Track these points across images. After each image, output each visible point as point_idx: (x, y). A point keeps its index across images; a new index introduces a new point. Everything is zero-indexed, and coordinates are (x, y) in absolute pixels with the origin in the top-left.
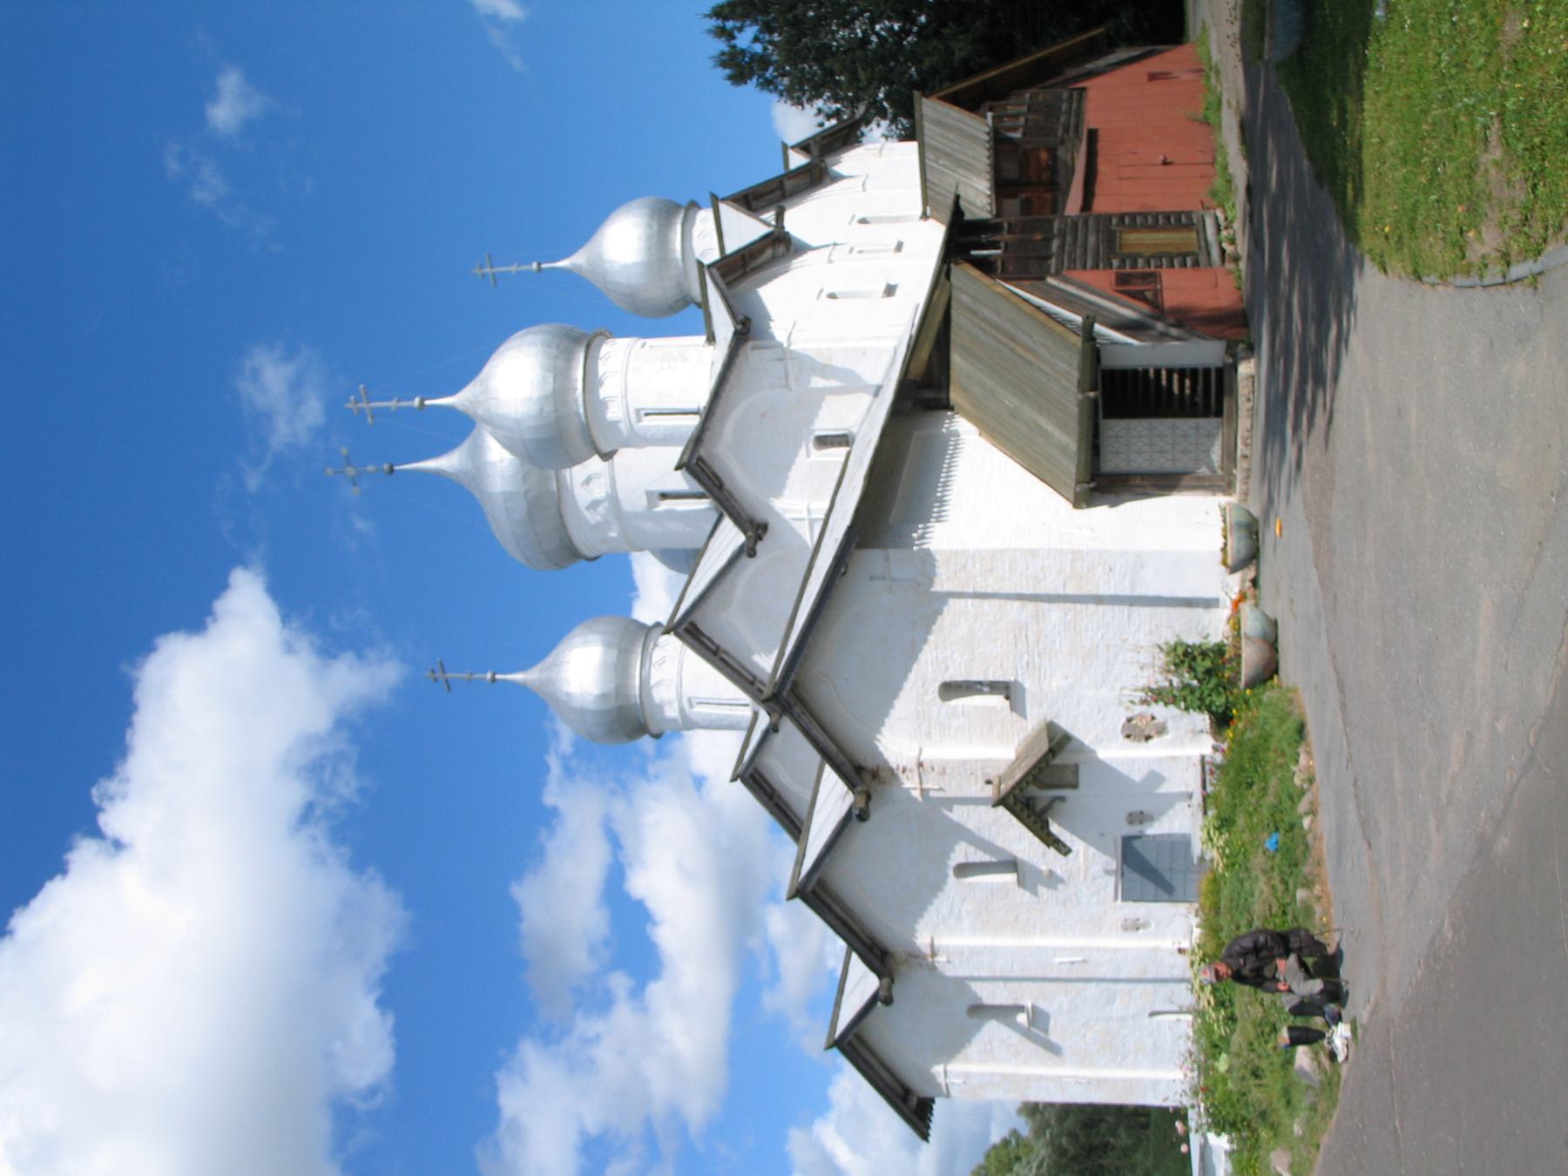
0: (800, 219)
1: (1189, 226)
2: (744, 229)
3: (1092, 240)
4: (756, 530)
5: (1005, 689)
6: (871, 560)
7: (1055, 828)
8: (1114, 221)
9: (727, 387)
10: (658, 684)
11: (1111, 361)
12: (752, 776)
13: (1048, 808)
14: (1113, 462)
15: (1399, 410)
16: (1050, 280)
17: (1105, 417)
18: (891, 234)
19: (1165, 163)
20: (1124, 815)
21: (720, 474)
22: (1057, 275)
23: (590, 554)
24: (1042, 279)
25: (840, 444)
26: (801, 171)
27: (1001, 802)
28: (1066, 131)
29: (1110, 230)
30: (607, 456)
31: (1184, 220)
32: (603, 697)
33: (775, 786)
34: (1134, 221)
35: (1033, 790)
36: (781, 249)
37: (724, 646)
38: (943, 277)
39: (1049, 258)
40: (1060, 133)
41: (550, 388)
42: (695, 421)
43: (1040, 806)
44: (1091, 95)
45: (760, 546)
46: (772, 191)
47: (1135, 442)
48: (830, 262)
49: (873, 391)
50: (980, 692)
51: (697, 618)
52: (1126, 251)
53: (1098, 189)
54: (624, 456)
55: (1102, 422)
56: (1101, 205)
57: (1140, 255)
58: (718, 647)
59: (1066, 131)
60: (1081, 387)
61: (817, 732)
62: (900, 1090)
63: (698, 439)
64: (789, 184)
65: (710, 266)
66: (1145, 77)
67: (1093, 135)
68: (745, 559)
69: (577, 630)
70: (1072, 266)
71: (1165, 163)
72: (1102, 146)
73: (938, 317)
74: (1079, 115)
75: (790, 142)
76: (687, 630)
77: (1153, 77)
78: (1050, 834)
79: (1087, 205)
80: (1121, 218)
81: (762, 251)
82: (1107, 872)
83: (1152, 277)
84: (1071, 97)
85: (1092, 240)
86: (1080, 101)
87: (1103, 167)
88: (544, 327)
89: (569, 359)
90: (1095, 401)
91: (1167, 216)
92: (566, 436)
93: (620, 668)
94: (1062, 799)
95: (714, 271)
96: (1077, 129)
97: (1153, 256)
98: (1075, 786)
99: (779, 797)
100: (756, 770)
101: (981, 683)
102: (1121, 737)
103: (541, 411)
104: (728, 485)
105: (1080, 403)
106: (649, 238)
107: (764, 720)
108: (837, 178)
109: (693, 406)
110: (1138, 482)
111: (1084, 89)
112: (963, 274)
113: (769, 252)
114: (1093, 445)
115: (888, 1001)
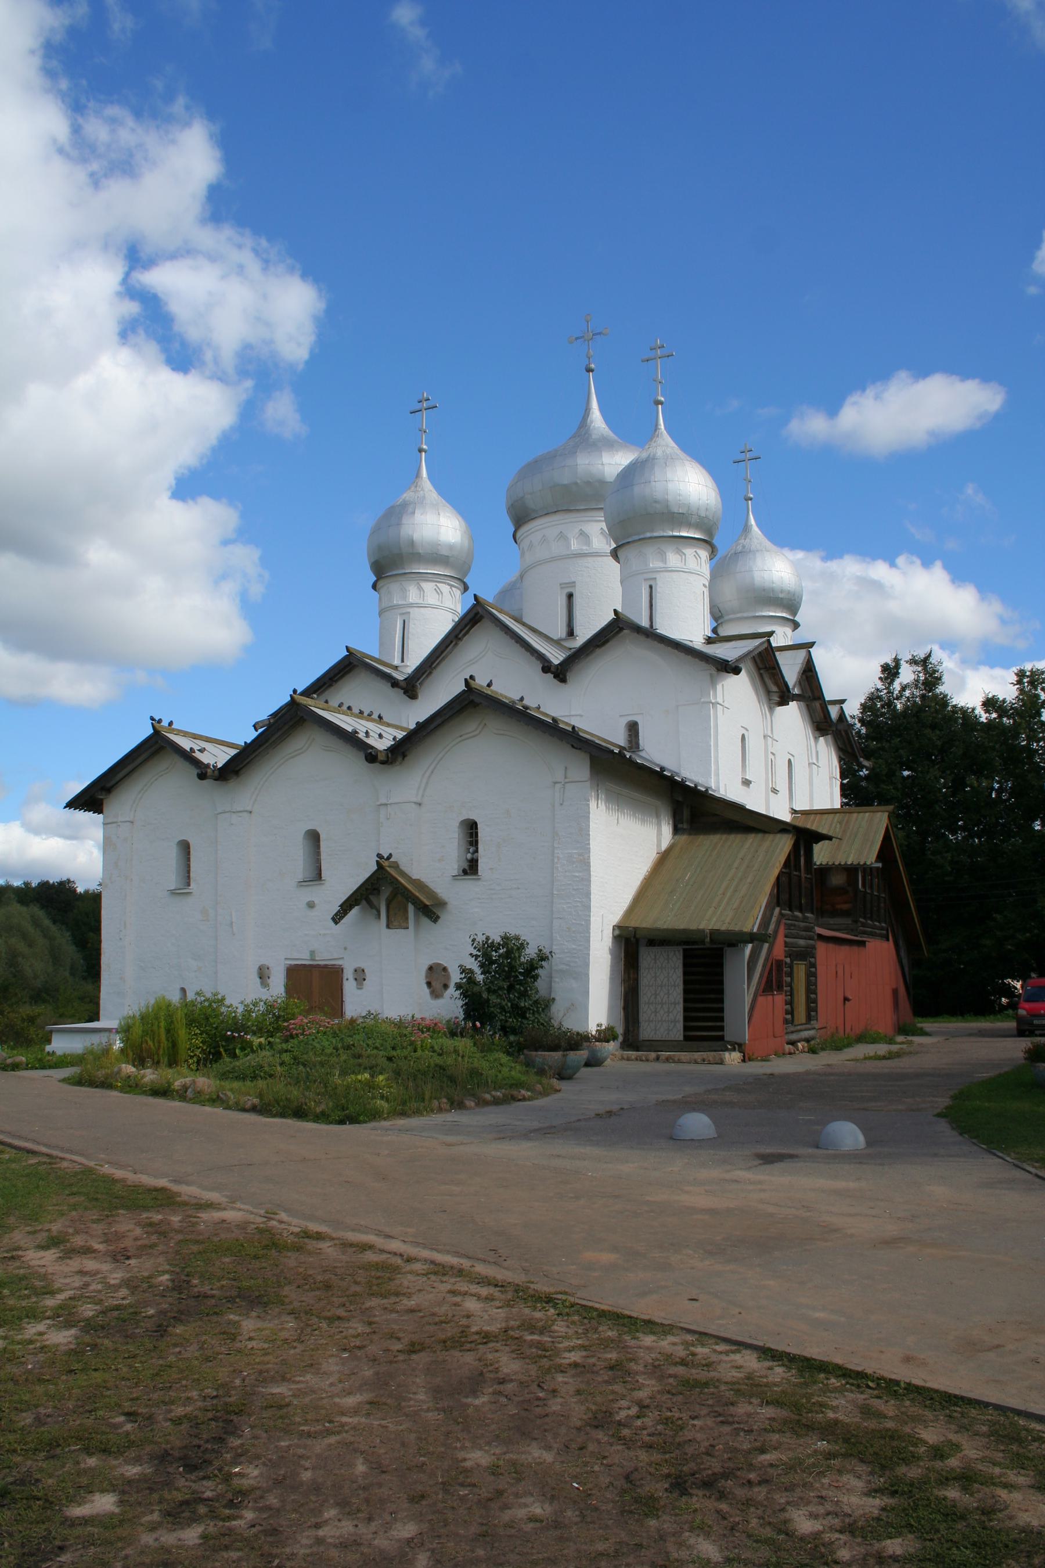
0: (792, 714)
1: (809, 1018)
3: (802, 942)
5: (471, 868)
6: (580, 768)
7: (355, 911)
8: (812, 960)
9: (682, 655)
10: (420, 589)
11: (728, 952)
12: (350, 663)
13: (371, 905)
14: (647, 957)
16: (777, 910)
17: (684, 950)
18: (782, 785)
19: (846, 999)
20: (362, 965)
21: (608, 645)
22: (781, 914)
23: (518, 535)
24: (778, 904)
25: (630, 742)
26: (826, 714)
29: (805, 955)
30: (615, 554)
31: (813, 1014)
32: (412, 543)
33: (340, 683)
34: (811, 976)
35: (386, 892)
36: (776, 698)
37: (461, 643)
38: (782, 827)
39: (790, 910)
42: (644, 623)
43: (372, 898)
45: (550, 676)
46: (812, 691)
47: (665, 981)
48: (765, 737)
51: (486, 623)
52: (795, 967)
53: (831, 946)
54: (613, 567)
55: (681, 948)
56: (821, 948)
57: (792, 979)
58: (460, 639)
60: (713, 932)
61: (439, 721)
62: (109, 785)
63: (650, 635)
64: (817, 704)
65: (769, 641)
67: (862, 944)
68: (539, 666)
69: (463, 524)
70: (788, 927)
71: (846, 999)
72: (855, 948)
73: (751, 824)
74: (873, 935)
76: (477, 614)
78: (351, 908)
79: (821, 937)
80: (814, 965)
81: (776, 684)
82: (312, 953)
83: (780, 988)
84: (882, 929)
85: (802, 942)
86: (881, 936)
87: (845, 949)
88: (720, 506)
90: (703, 942)
91: (815, 1001)
92: (641, 525)
93: (437, 557)
95: (766, 645)
96: (864, 933)
97: (792, 988)
98: (388, 927)
99: (331, 686)
100: (355, 666)
101: (476, 851)
102: (431, 963)
103: (656, 502)
104: (598, 651)
105: (703, 931)
106: (773, 590)
107: (400, 677)
108: (816, 739)
111: (888, 940)
112: (784, 844)
113: (774, 688)
114: (660, 940)
115: (202, 776)
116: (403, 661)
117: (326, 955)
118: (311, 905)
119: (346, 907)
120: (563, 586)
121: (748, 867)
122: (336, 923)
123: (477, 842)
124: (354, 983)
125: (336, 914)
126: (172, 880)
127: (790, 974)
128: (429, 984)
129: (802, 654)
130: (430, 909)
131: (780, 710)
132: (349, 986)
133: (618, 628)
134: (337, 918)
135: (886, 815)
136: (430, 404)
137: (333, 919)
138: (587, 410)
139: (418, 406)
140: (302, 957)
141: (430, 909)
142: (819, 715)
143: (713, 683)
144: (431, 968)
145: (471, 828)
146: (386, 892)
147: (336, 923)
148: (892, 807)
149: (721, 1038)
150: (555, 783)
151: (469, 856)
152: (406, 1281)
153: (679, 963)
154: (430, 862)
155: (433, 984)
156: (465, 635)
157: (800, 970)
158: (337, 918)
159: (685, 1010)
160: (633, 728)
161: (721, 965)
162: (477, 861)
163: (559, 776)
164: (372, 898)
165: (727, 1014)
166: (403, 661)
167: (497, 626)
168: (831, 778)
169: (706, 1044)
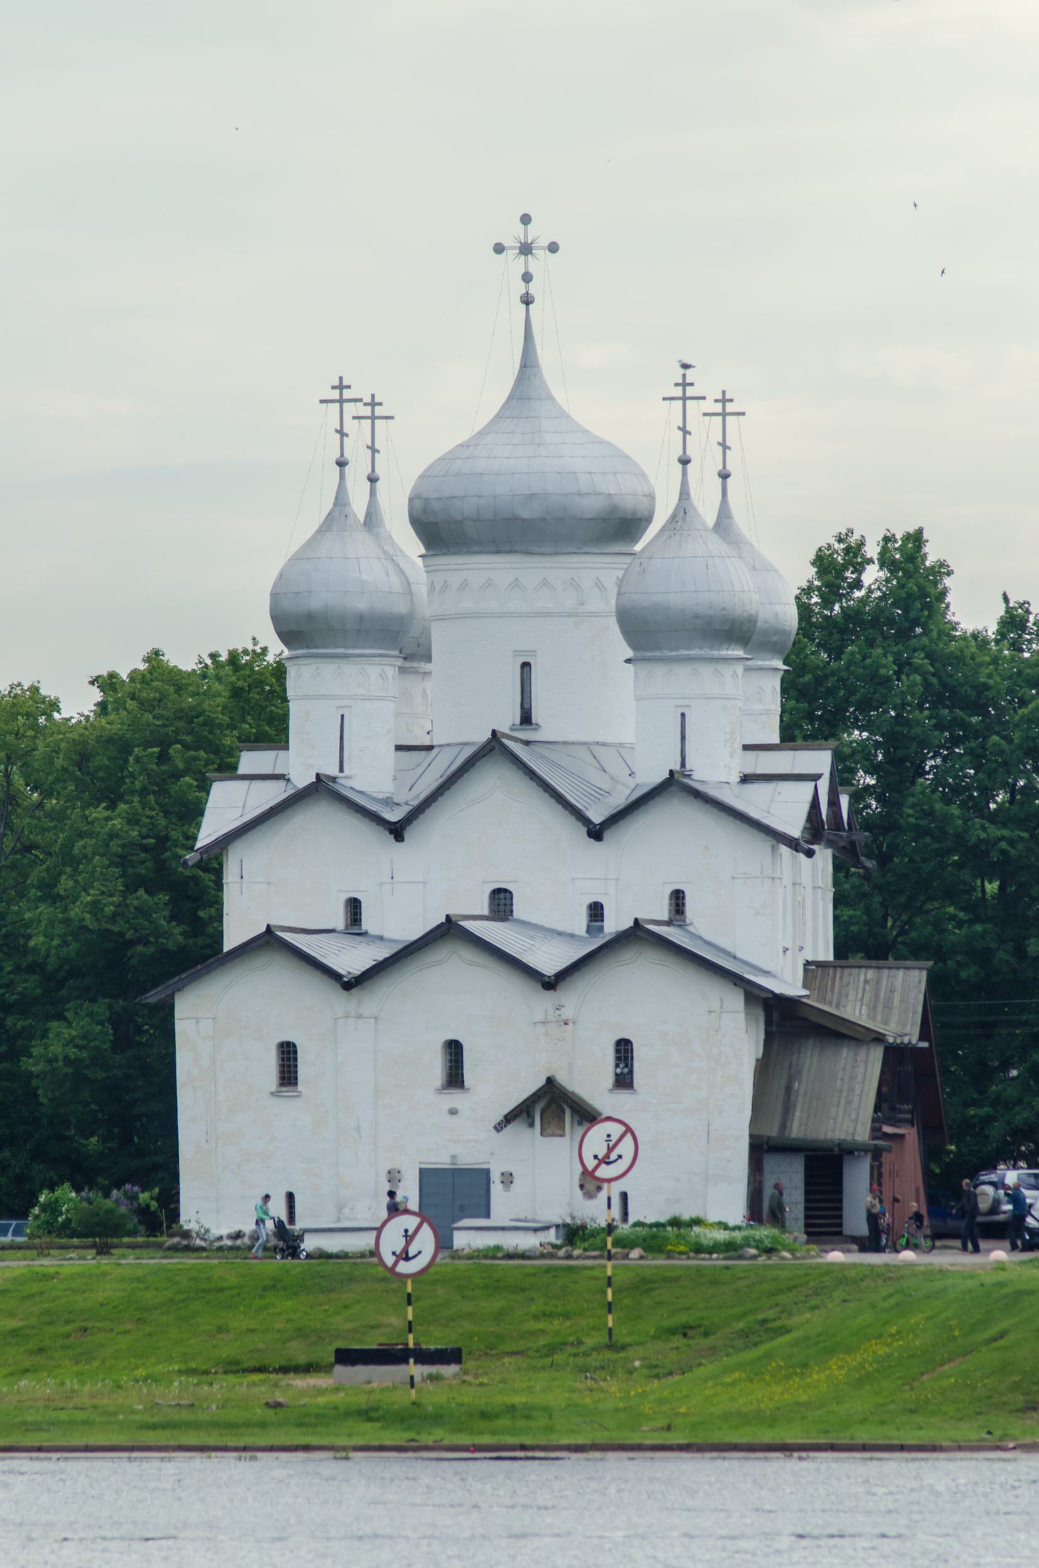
4: (596, 833)
19: (896, 1200)
38: (875, 1035)
47: (790, 1179)
55: (803, 1155)
73: (844, 1031)
82: (454, 1157)
90: (832, 1150)
116: (341, 770)
117: (469, 1159)
118: (453, 1112)
119: (509, 1118)
120: (517, 653)
121: (851, 1077)
124: (501, 1186)
128: (582, 1187)
129: (812, 784)
130: (588, 1116)
132: (496, 1188)
134: (499, 1127)
135: (924, 974)
137: (495, 1128)
140: (440, 1159)
141: (588, 1116)
147: (498, 1131)
148: (931, 963)
149: (840, 1233)
150: (382, 884)
154: (591, 1082)
158: (499, 1127)
159: (806, 1209)
160: (678, 899)
163: (716, 1006)
165: (846, 1213)
166: (341, 770)
167: (519, 768)
169: (830, 1238)
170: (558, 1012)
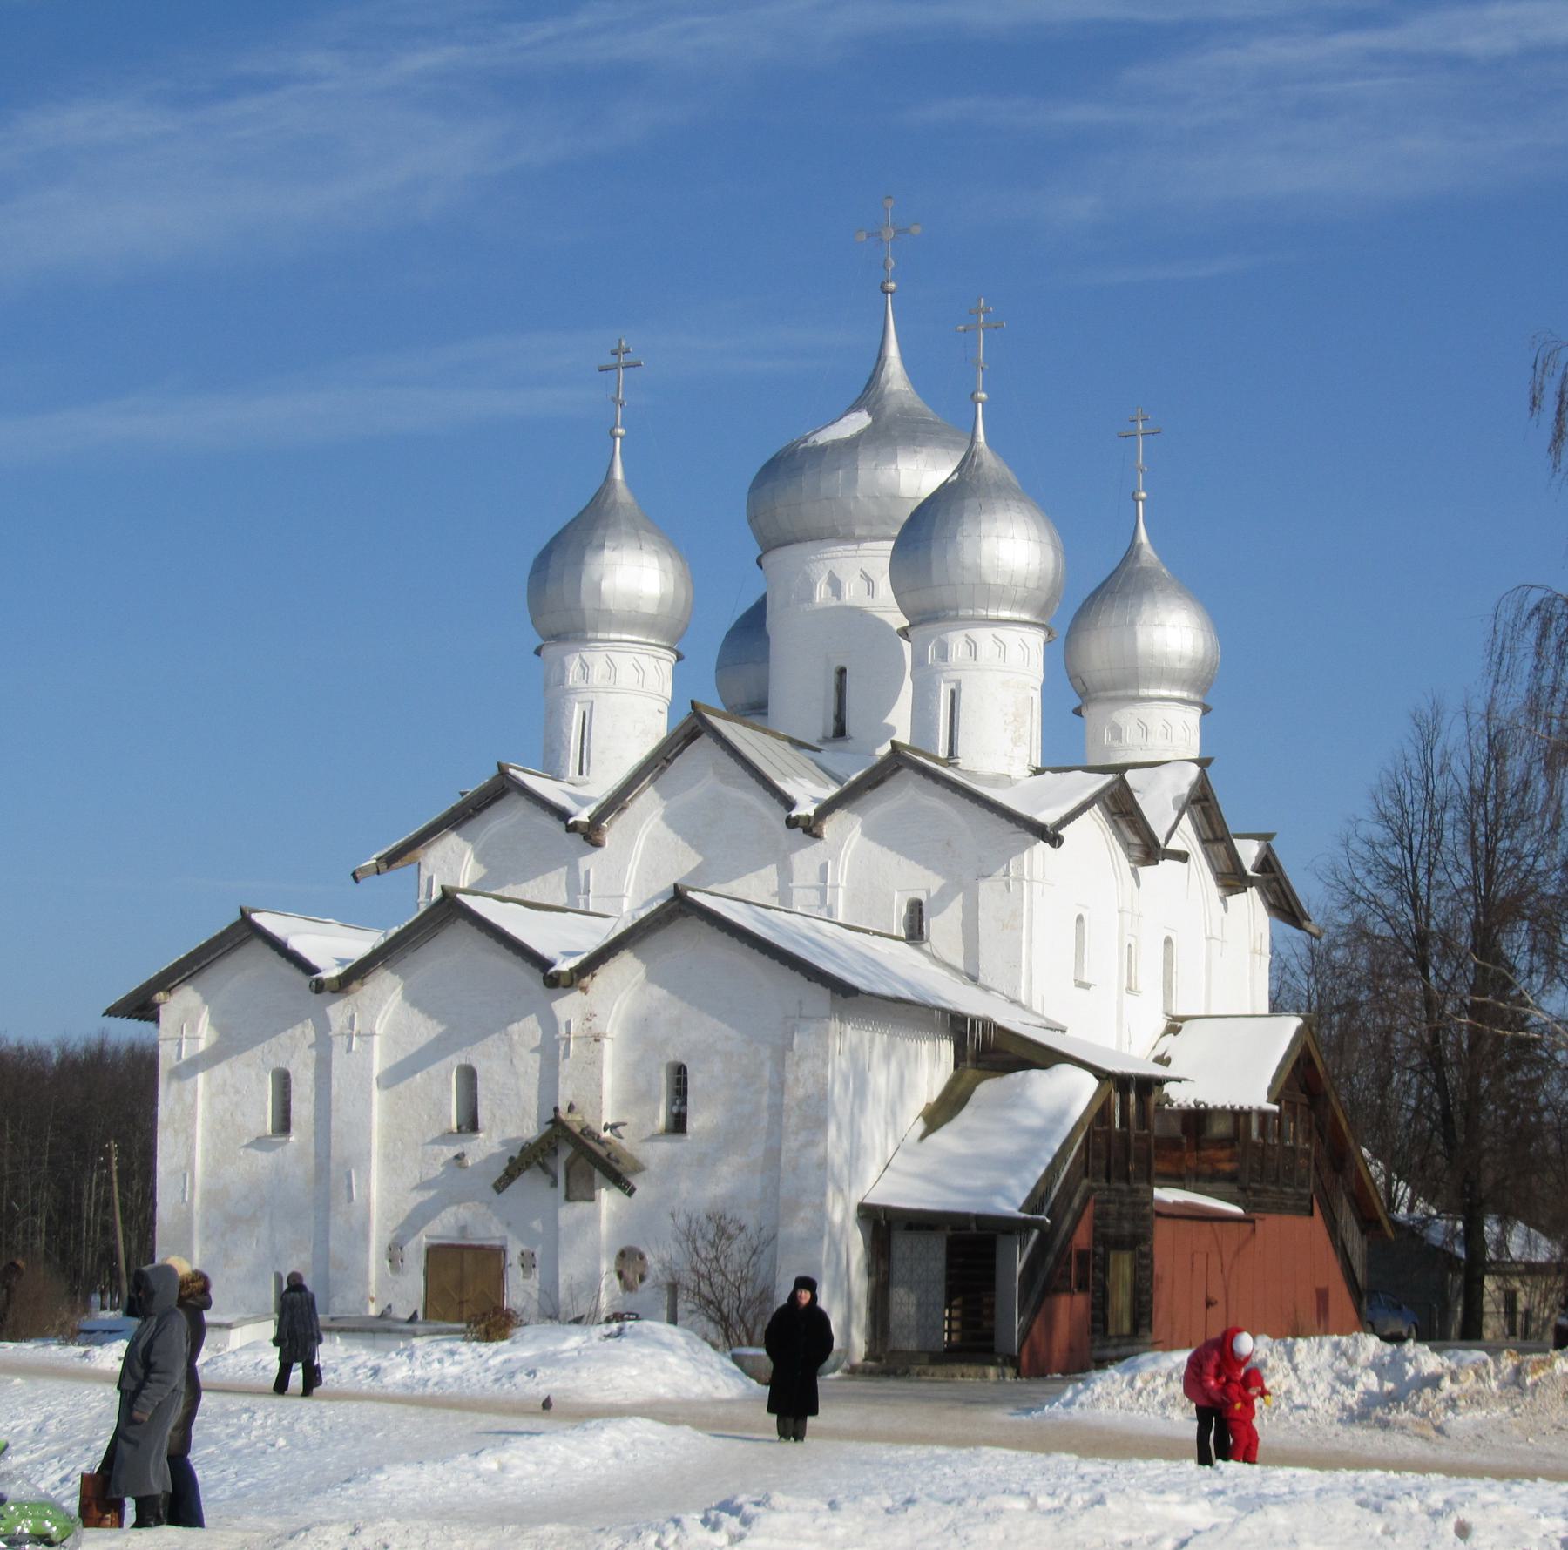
2: (1160, 800)
11: (1002, 1243)
13: (544, 1167)
14: (902, 1244)
15: (1534, 403)
27: (556, 1122)
28: (1256, 1192)
35: (566, 1152)
40: (1255, 1185)
41: (991, 580)
43: (549, 1162)
44: (1302, 1222)
47: (926, 1261)
49: (972, 972)
50: (672, 1103)
51: (705, 741)
59: (1256, 1192)
65: (1123, 781)
66: (1322, 1285)
75: (1273, 843)
77: (1322, 1296)
81: (1137, 833)
89: (1021, 604)
94: (554, 1184)
101: (685, 1103)
109: (961, 750)
110: (882, 1268)
111: (1311, 1214)
113: (1137, 841)
122: (499, 1191)
123: (685, 1091)
125: (499, 1181)
126: (267, 1122)
127: (1105, 1269)
128: (620, 1275)
131: (1145, 872)
133: (898, 760)
136: (631, 358)
138: (881, 357)
139: (613, 360)
142: (1224, 865)
143: (1028, 845)
144: (622, 1254)
145: (679, 1072)
146: (566, 1152)
147: (499, 1191)
151: (675, 1109)
152: (667, 1258)
153: (941, 1253)
155: (625, 1272)
156: (676, 755)
157: (1122, 1266)
161: (993, 1256)
162: (685, 1116)
164: (549, 1162)
168: (1254, 952)
170: (588, 1024)
